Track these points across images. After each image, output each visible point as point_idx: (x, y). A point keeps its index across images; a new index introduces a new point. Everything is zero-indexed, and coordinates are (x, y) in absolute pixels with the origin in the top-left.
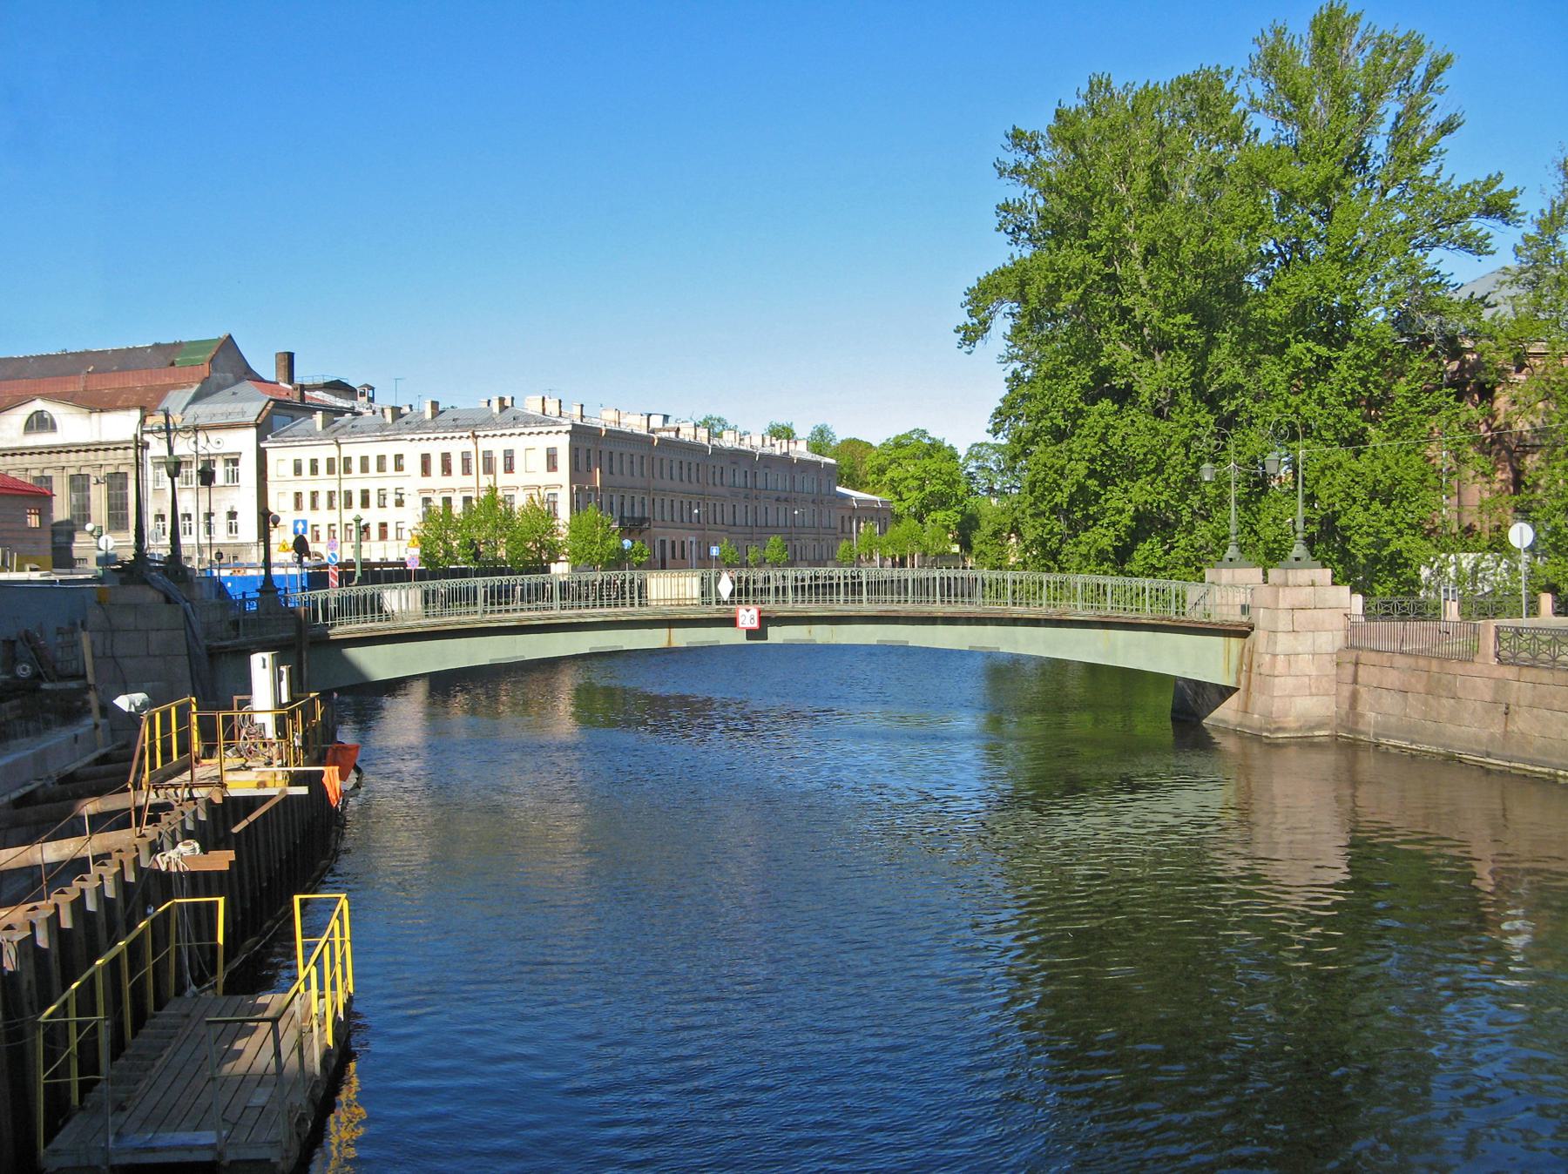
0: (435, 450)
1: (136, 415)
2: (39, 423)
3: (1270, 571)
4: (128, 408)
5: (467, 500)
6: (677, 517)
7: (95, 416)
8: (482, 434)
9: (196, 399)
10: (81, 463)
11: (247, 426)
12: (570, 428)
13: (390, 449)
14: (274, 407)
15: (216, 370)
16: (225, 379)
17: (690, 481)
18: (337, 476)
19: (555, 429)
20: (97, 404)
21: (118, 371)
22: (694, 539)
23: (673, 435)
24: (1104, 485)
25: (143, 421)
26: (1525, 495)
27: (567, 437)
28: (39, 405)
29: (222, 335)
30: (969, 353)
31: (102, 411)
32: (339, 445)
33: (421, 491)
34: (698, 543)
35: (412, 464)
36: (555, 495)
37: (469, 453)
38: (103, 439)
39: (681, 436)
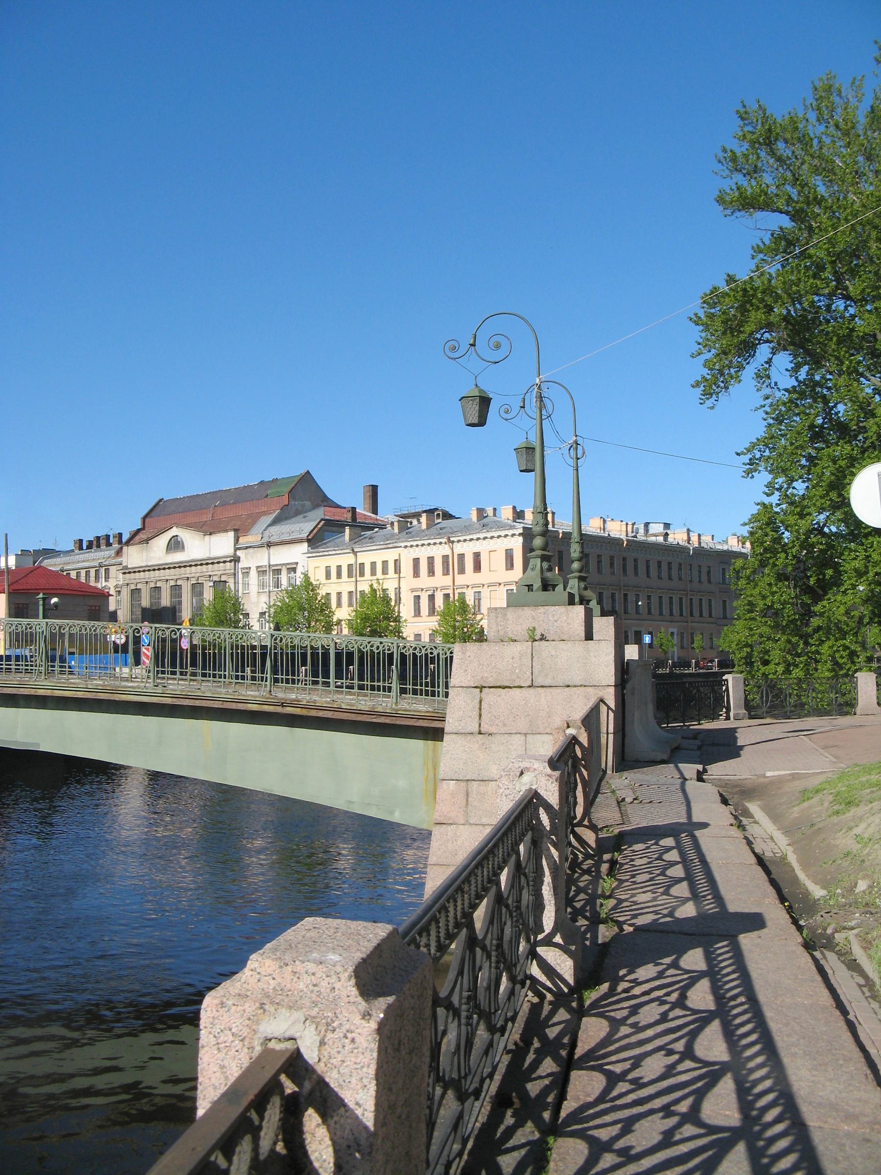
0: (423, 553)
1: (231, 534)
2: (175, 545)
3: (599, 827)
4: (226, 531)
5: (447, 596)
6: (666, 611)
7: (207, 537)
8: (455, 539)
9: (274, 522)
10: (198, 575)
11: (300, 541)
12: (521, 531)
13: (390, 555)
14: (324, 525)
15: (295, 499)
16: (303, 506)
17: (636, 573)
18: (354, 579)
19: (510, 532)
20: (209, 529)
21: (233, 503)
22: (675, 630)
23: (661, 539)
24: (278, 572)
25: (237, 540)
26: (485, 521)
27: (521, 539)
28: (174, 531)
29: (303, 471)
30: (712, 408)
31: (210, 534)
32: (355, 553)
33: (413, 590)
34: (681, 635)
35: (407, 568)
36: (480, 592)
37: (448, 556)
38: (212, 556)
39: (671, 539)
